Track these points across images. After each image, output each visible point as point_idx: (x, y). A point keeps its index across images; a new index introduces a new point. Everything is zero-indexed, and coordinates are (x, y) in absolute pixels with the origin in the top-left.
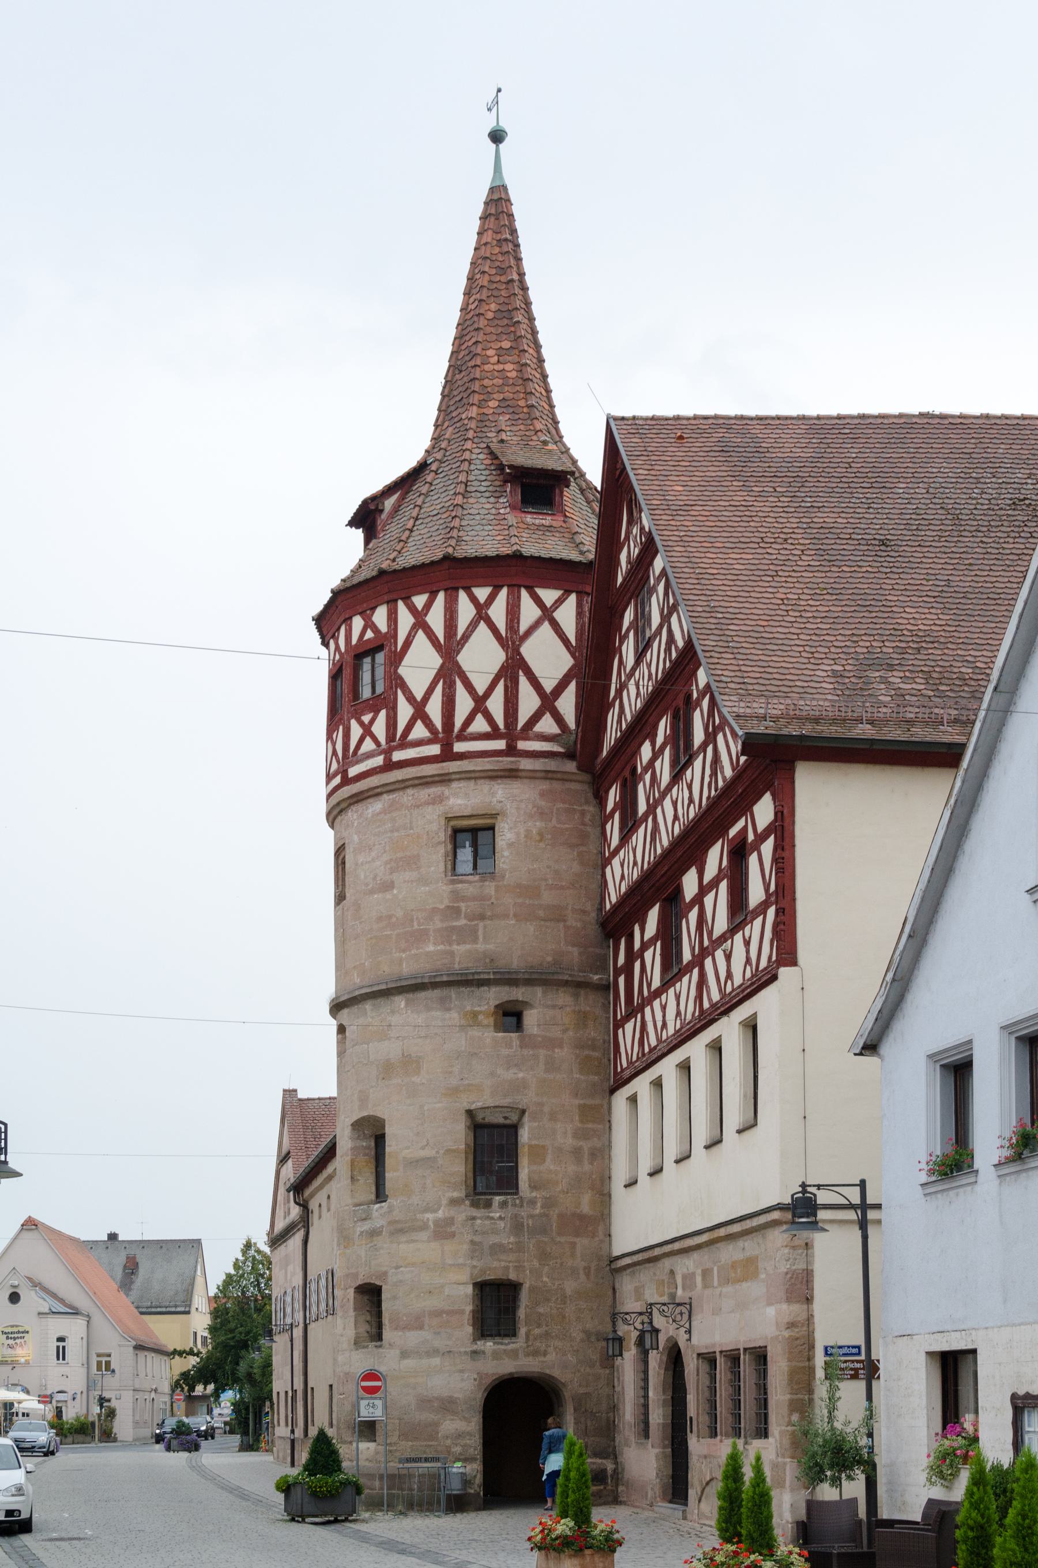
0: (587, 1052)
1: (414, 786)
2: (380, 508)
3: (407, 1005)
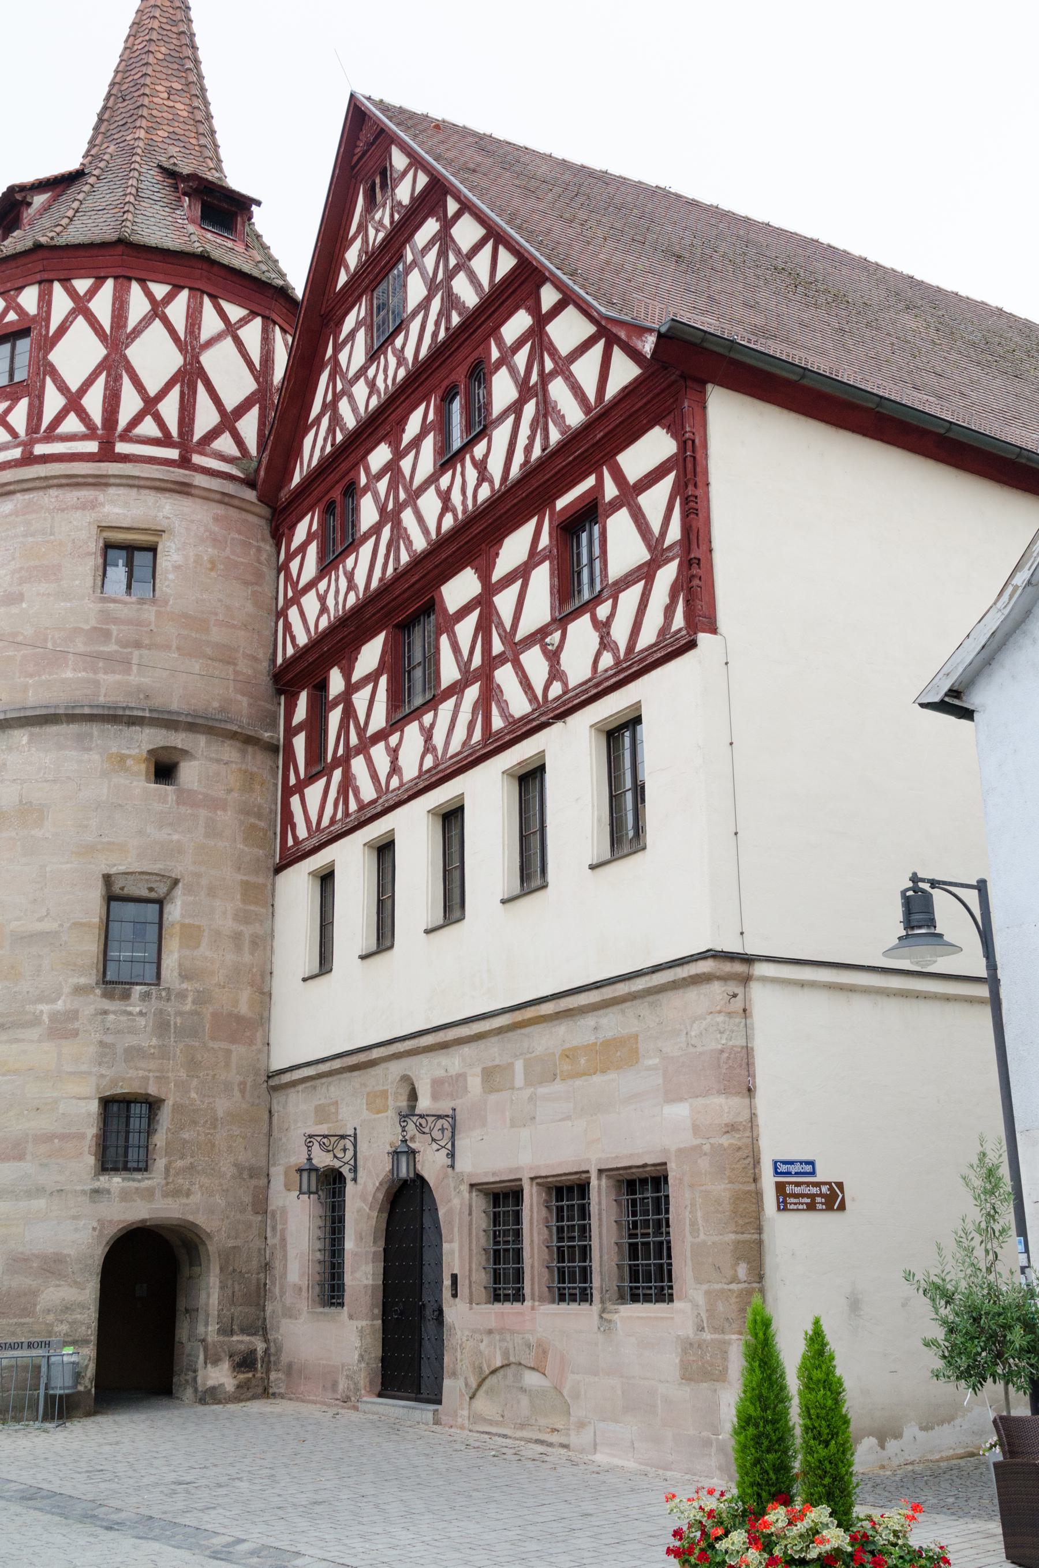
0: (252, 820)
1: (60, 486)
2: (29, 200)
3: (30, 742)
